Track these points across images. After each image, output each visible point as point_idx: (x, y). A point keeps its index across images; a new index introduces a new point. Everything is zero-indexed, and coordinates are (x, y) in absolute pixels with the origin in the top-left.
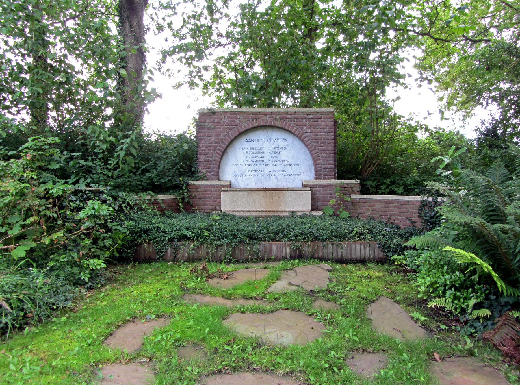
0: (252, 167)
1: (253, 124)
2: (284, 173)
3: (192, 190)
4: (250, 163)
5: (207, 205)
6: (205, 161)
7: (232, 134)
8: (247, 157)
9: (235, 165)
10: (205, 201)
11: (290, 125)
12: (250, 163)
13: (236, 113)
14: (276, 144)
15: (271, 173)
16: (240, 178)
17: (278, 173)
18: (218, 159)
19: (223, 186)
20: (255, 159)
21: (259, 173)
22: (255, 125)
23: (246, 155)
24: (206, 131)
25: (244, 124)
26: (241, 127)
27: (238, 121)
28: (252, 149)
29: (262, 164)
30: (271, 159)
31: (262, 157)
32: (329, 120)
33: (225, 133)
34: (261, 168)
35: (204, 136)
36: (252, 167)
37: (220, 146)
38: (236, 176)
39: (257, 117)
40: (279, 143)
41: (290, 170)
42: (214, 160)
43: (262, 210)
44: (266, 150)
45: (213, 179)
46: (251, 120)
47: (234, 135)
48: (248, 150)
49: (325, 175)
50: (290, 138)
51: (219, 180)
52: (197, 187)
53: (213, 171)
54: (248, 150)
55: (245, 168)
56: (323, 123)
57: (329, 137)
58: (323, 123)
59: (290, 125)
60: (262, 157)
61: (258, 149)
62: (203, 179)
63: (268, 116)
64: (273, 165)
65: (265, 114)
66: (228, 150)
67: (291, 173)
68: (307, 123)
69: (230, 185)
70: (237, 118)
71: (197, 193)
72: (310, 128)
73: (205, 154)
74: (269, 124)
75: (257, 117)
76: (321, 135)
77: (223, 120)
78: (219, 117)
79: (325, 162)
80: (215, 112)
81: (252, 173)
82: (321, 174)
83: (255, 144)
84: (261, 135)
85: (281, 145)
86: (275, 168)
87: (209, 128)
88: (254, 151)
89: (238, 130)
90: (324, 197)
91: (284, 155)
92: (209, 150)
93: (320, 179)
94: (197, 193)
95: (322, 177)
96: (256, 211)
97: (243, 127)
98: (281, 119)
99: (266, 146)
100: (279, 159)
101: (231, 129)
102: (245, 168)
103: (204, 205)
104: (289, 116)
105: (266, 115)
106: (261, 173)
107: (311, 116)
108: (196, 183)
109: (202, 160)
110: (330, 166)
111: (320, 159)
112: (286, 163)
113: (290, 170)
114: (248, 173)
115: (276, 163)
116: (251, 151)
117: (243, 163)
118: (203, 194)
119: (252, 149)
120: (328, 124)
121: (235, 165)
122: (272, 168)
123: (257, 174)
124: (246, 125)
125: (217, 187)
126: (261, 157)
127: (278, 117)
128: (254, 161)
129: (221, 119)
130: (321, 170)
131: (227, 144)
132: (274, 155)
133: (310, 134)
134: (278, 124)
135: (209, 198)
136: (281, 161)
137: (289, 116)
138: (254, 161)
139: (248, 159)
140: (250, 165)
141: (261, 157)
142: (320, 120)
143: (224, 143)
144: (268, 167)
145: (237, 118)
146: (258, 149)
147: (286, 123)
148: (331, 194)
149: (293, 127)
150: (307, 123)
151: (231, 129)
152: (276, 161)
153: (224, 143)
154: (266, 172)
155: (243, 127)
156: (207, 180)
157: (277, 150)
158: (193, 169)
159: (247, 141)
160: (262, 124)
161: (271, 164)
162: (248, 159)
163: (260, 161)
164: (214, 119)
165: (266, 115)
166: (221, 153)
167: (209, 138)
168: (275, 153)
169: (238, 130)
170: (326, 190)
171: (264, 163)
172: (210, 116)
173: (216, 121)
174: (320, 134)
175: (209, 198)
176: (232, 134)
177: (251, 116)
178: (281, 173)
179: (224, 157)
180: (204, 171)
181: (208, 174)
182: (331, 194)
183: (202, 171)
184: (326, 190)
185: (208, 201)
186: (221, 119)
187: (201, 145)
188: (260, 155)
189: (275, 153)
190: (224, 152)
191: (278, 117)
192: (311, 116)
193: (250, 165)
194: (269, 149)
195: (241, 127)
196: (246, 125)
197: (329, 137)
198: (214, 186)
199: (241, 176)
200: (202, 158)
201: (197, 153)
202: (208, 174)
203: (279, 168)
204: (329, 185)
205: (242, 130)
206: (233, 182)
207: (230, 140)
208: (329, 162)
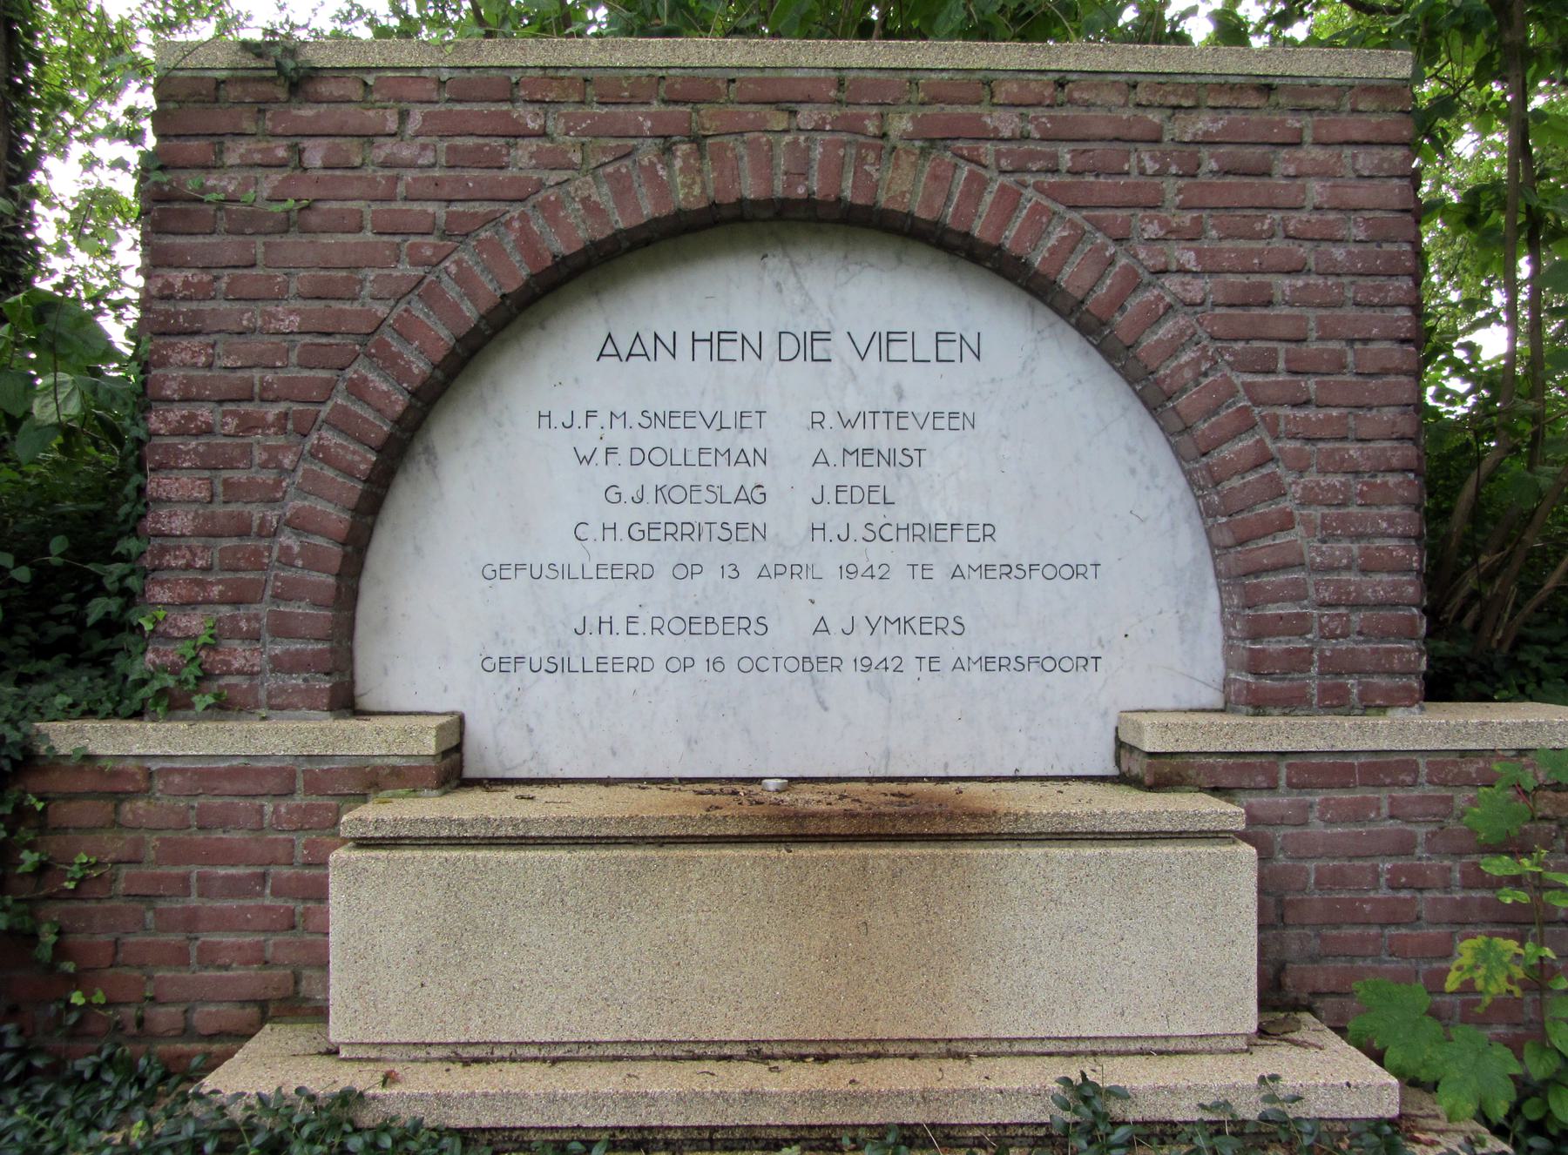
0: (662, 585)
1: (663, 189)
2: (950, 647)
3: (67, 812)
4: (639, 553)
5: (209, 957)
6: (208, 532)
7: (464, 279)
8: (612, 493)
9: (499, 573)
10: (191, 922)
11: (1009, 201)
12: (639, 553)
13: (505, 86)
14: (870, 385)
15: (834, 645)
16: (547, 688)
17: (890, 644)
18: (336, 516)
19: (373, 780)
20: (684, 513)
21: (718, 644)
22: (687, 193)
23: (602, 474)
24: (224, 245)
25: (583, 186)
26: (550, 211)
27: (523, 152)
28: (654, 419)
29: (751, 556)
30: (835, 516)
31: (752, 496)
32: (1366, 160)
33: (405, 269)
34: (744, 597)
35: (205, 293)
36: (662, 585)
37: (357, 390)
38: (506, 665)
39: (708, 118)
40: (910, 375)
41: (1005, 616)
42: (298, 524)
43: (758, 1053)
44: (785, 435)
45: (279, 705)
46: (648, 152)
47: (491, 289)
48: (619, 437)
49: (1335, 667)
50: (1004, 329)
51: (346, 703)
52: (118, 785)
53: (282, 629)
54: (619, 437)
55: (589, 596)
56: (1316, 190)
57: (1374, 322)
58: (1316, 190)
59: (1009, 201)
60: (752, 496)
61: (716, 422)
62: (174, 704)
63: (807, 116)
64: (849, 571)
65: (782, 96)
66: (440, 434)
67: (1017, 642)
68: (1171, 188)
69: (452, 769)
70: (518, 134)
71: (115, 845)
72: (1192, 236)
73: (210, 463)
74: (815, 184)
75: (708, 118)
76: (1299, 299)
77: (386, 148)
78: (351, 116)
79: (1341, 549)
80: (313, 74)
81: (659, 647)
82: (1298, 661)
83: (685, 380)
84: (737, 295)
85: (925, 387)
86: (871, 598)
87: (248, 223)
88: (680, 440)
89: (528, 243)
90: (1337, 879)
91: (945, 482)
92: (248, 425)
93: (1292, 703)
94: (115, 845)
95: (1313, 681)
96: (693, 1053)
97: (573, 212)
98: (932, 141)
99: (788, 390)
100: (902, 515)
101: (456, 232)
102: (589, 596)
103: (180, 958)
104: (1005, 122)
105: (787, 104)
106: (744, 645)
107: (1202, 124)
108: (107, 739)
109: (181, 522)
110: (1379, 584)
111: (1287, 523)
112: (967, 553)
113: (1005, 616)
114: (621, 646)
115: (877, 553)
116: (647, 439)
117: (571, 554)
118: (176, 853)
119: (654, 419)
120: (1360, 194)
121: (499, 573)
122: (840, 599)
123: (700, 648)
124: (603, 195)
125: (315, 784)
126: (743, 496)
127: (901, 124)
128: (677, 531)
129: (368, 137)
130: (1298, 626)
131: (420, 367)
132: (863, 477)
133: (1197, 289)
134: (903, 187)
135: (234, 887)
136: (930, 532)
137: (1005, 122)
138: (677, 531)
139: (625, 515)
140: (636, 572)
141: (743, 496)
142: (1284, 164)
143: (389, 363)
144: (801, 588)
145: (518, 134)
146: (716, 422)
147: (977, 185)
148: (1405, 846)
149: (1039, 223)
150: (1171, 188)
151: (456, 232)
152: (876, 534)
153: (389, 363)
154: (789, 634)
155: (573, 212)
156: (224, 707)
157: (882, 438)
158: (97, 608)
159: (608, 349)
160: (750, 188)
161: (830, 557)
162: (625, 515)
163: (732, 533)
164: (297, 137)
165: (787, 104)
166: (365, 460)
167: (249, 316)
168: (875, 454)
169: (528, 243)
170: (1357, 814)
171: (766, 554)
172: (261, 107)
173: (315, 154)
174: (1283, 285)
175: (234, 887)
176: (464, 279)
177: (643, 117)
178: (927, 646)
179: (403, 497)
180: (196, 622)
181: (240, 654)
182: (1405, 846)
183: (174, 620)
184: (1357, 814)
185: (225, 922)
186: (368, 137)
187: (171, 380)
188: (731, 478)
189: (875, 454)
190: (398, 450)
191: (901, 124)
192: (1202, 124)
193: (636, 572)
194: (817, 421)
195: (550, 211)
196: (603, 195)
197: (1374, 322)
198: (282, 779)
199: (558, 666)
200: (178, 500)
201: (137, 458)
202: (240, 654)
203: (904, 597)
204: (1383, 768)
205: (557, 245)
206: (479, 730)
207: (444, 335)
208: (1369, 552)
